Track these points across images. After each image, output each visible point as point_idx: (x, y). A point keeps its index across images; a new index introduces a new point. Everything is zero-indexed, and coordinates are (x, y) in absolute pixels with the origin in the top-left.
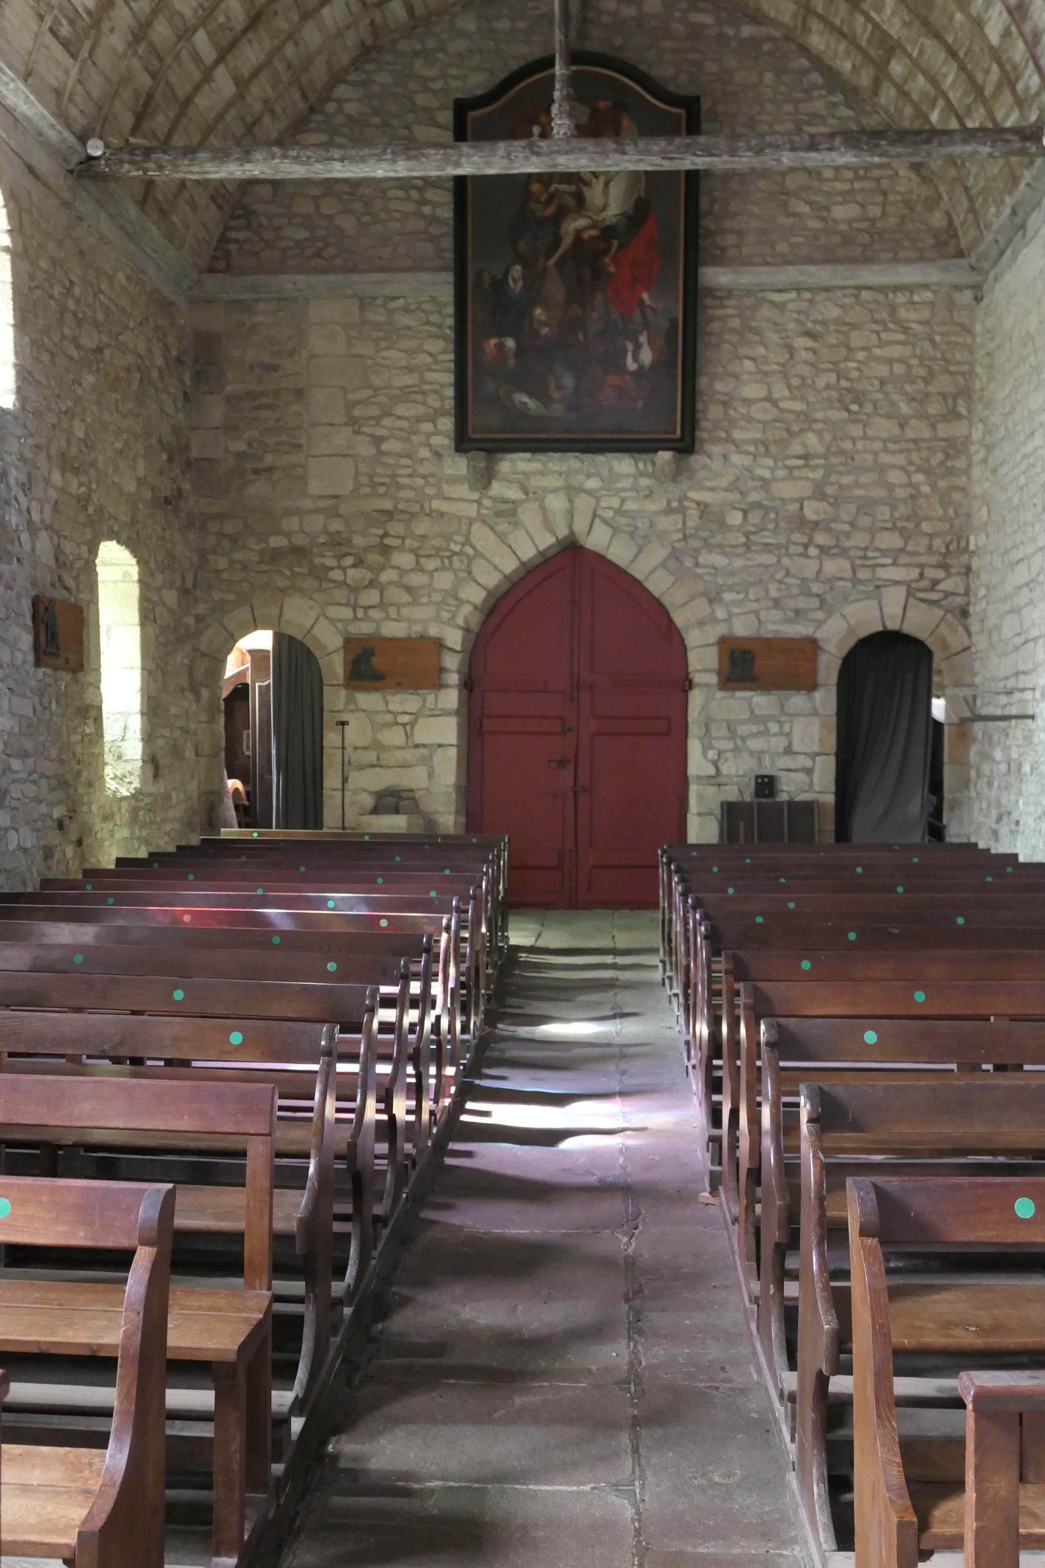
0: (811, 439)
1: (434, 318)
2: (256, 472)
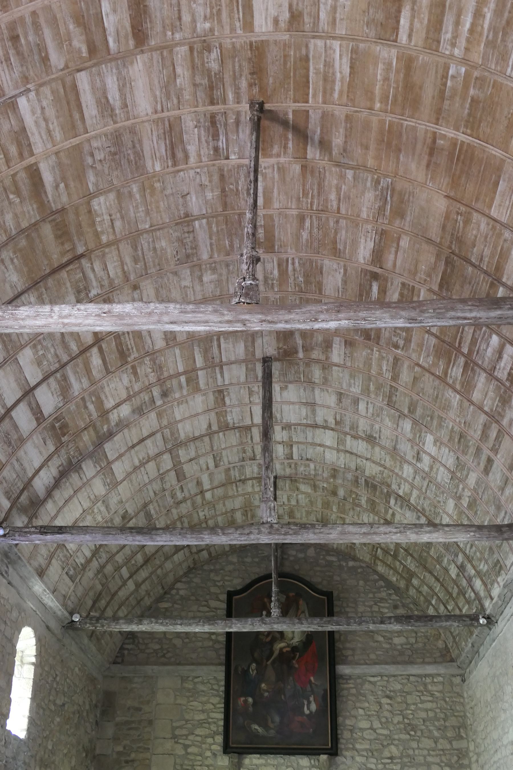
0: (393, 748)
1: (216, 687)
2: (127, 762)
